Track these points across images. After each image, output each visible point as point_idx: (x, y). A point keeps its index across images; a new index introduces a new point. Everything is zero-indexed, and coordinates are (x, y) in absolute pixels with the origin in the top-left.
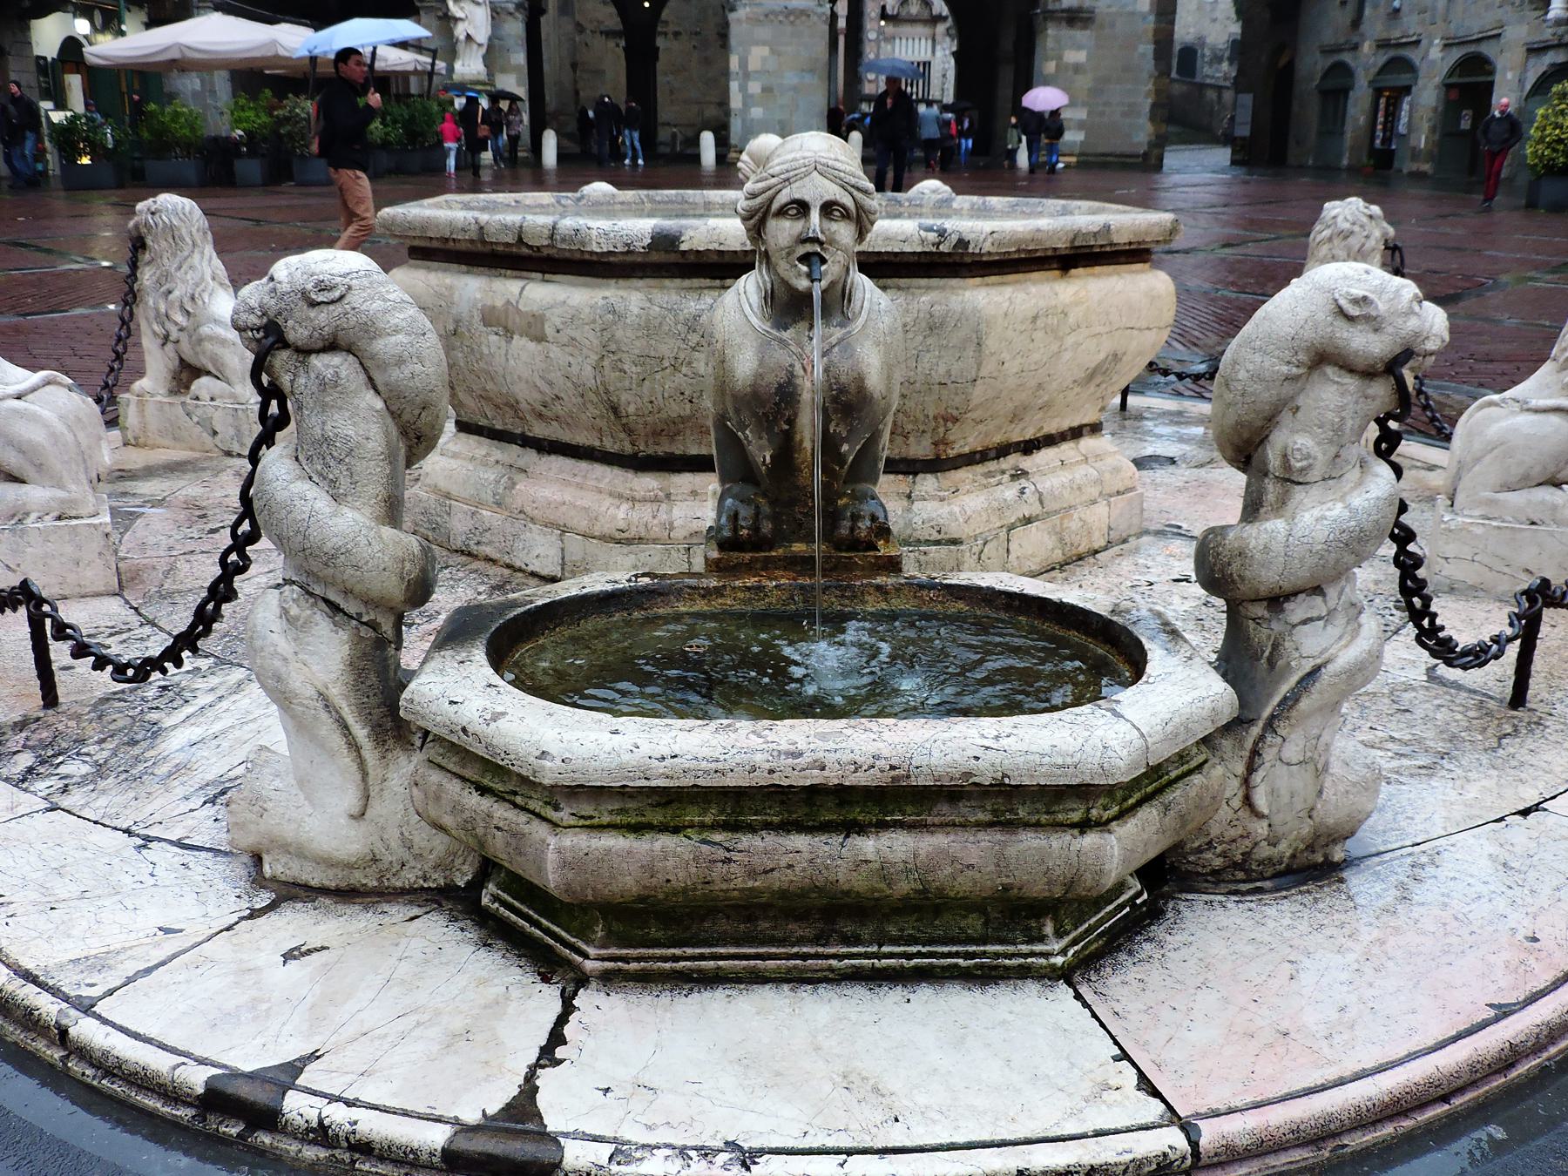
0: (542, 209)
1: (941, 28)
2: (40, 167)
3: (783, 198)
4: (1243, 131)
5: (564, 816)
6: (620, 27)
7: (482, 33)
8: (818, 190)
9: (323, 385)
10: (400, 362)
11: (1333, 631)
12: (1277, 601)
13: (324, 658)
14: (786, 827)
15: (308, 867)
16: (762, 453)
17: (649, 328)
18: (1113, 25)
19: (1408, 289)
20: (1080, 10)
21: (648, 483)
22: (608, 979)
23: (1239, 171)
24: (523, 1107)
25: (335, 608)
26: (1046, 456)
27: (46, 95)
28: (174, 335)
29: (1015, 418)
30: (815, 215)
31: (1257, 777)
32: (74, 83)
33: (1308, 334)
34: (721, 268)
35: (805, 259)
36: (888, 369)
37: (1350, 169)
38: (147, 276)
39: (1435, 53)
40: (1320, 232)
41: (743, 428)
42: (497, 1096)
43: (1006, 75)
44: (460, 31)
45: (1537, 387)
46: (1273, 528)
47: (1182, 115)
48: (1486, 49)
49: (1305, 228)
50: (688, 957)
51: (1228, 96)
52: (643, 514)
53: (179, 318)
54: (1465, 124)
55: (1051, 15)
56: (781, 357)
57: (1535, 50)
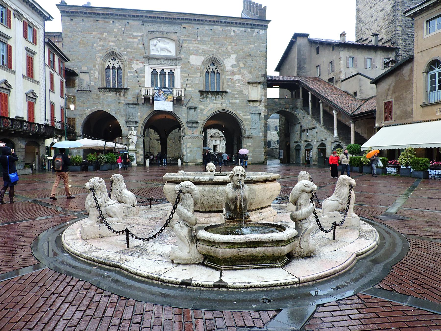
0: (192, 175)
1: (222, 138)
2: (44, 168)
3: (236, 174)
4: (281, 157)
5: (221, 247)
6: (159, 139)
7: (135, 141)
8: (240, 173)
9: (187, 197)
10: (196, 194)
11: (308, 224)
12: (301, 221)
13: (184, 232)
14: (247, 247)
15: (181, 261)
16: (232, 207)
17: (209, 192)
18: (256, 138)
19: (312, 183)
20: (250, 136)
21: (207, 215)
22: (225, 270)
23: (282, 165)
24: (221, 280)
25: (187, 225)
26: (263, 210)
27: (47, 154)
28: (118, 196)
29: (259, 204)
30: (240, 176)
31: (301, 243)
32: (53, 151)
33: (301, 188)
34: (224, 183)
35: (239, 181)
36: (248, 195)
37: (302, 164)
38: (114, 187)
39: (315, 143)
40: (299, 176)
41: (230, 203)
42: (218, 279)
43: (236, 147)
44: (131, 141)
45: (333, 197)
46: (299, 212)
47: (270, 155)
48: (324, 142)
49: (297, 175)
50: (234, 267)
51: (278, 150)
52: (207, 219)
53: (119, 194)
54: (322, 155)
55: (244, 137)
56: (236, 194)
57: (333, 142)
